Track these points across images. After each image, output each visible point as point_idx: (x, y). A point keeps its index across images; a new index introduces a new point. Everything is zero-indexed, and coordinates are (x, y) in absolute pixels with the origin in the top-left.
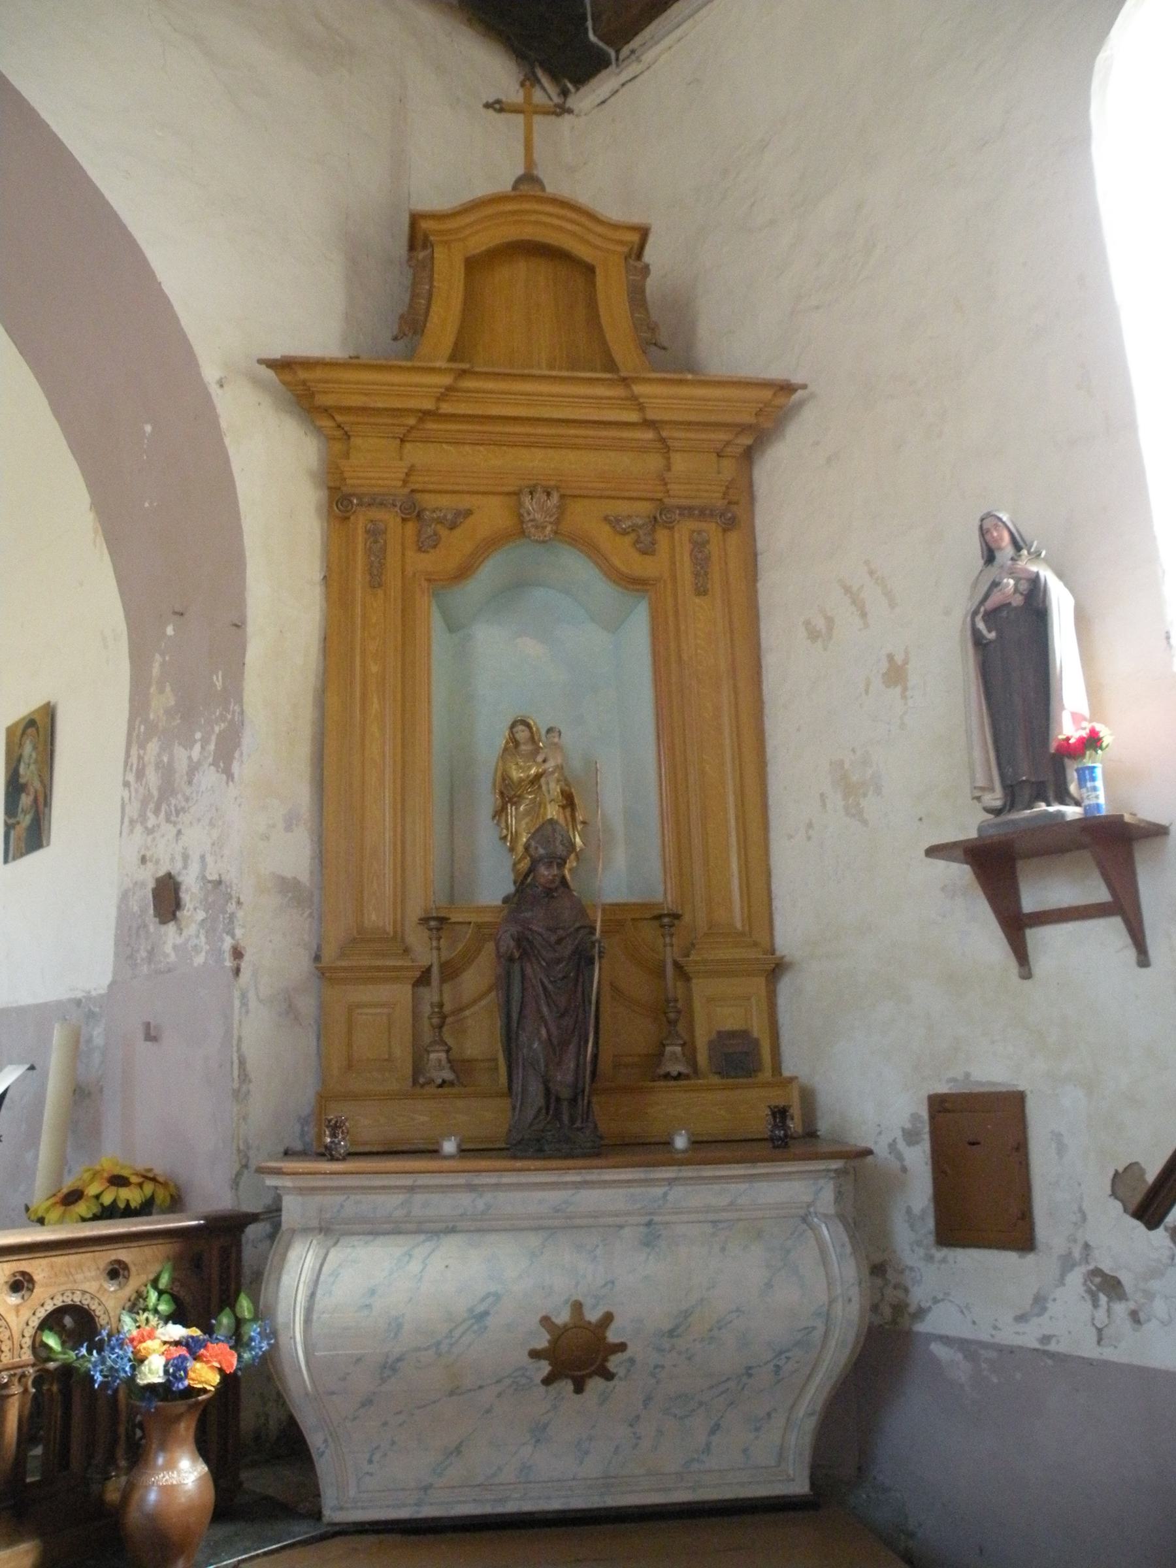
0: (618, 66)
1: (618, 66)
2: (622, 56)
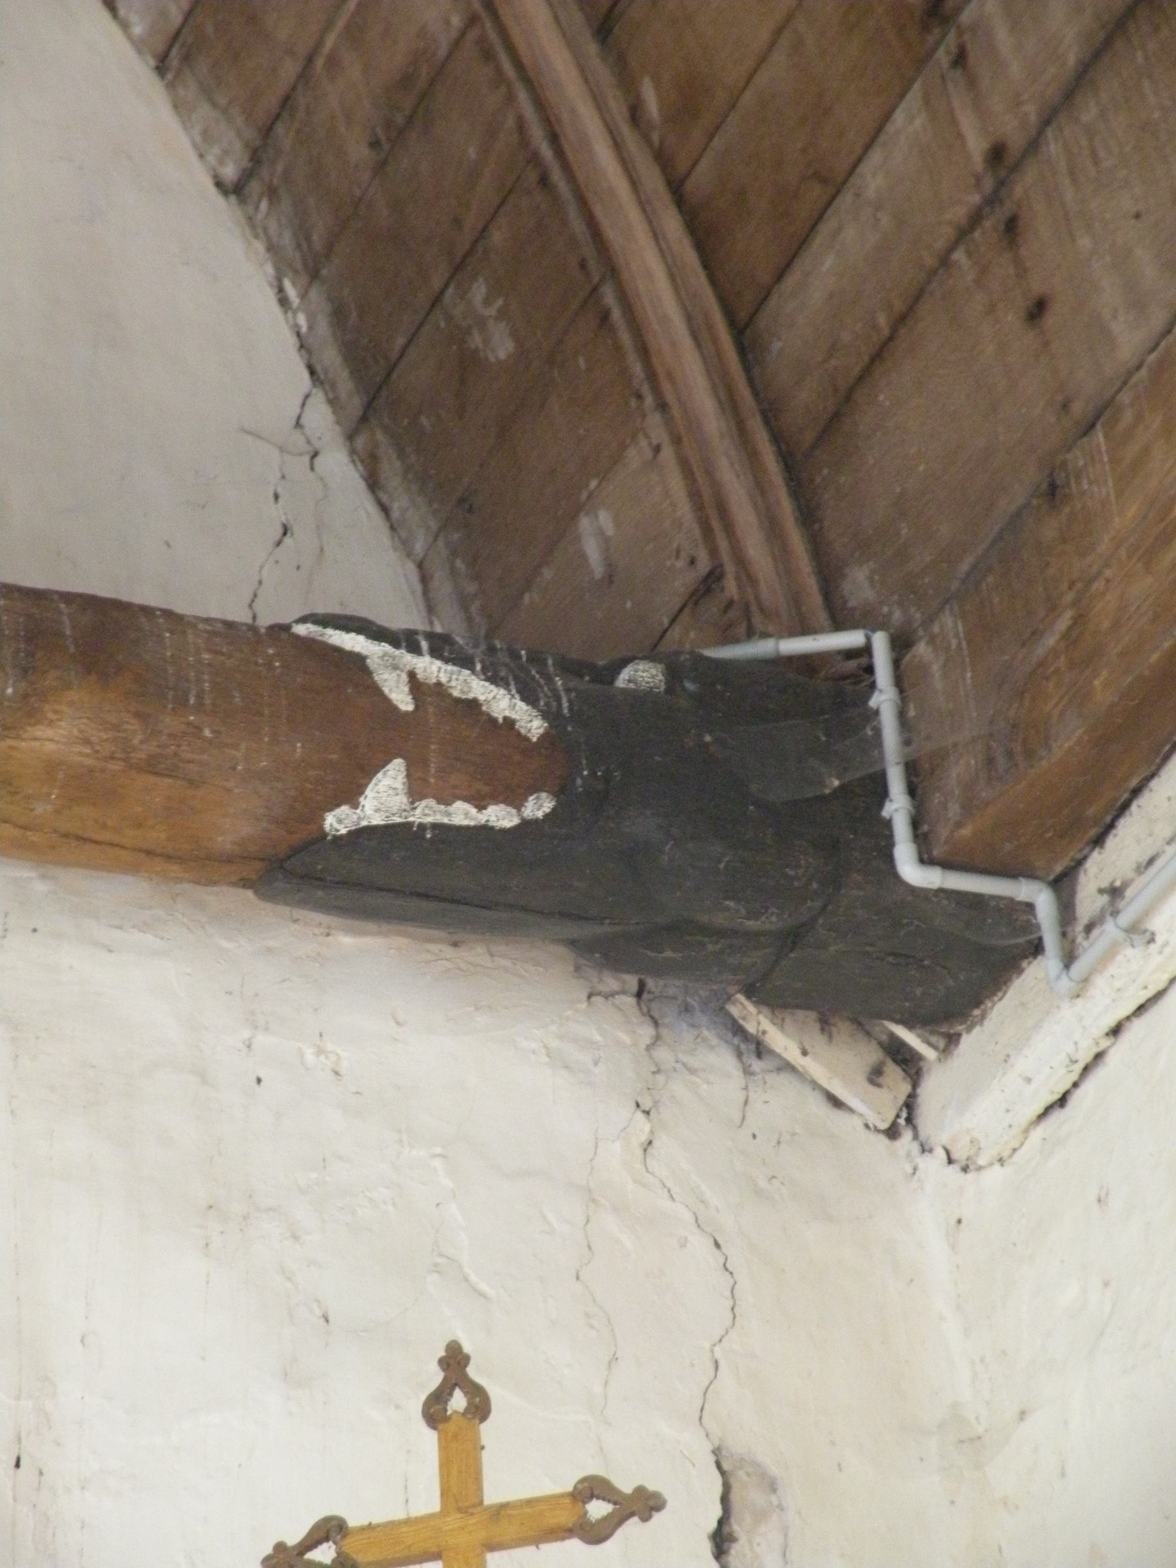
0: (1069, 958)
1: (1069, 958)
2: (1088, 899)
